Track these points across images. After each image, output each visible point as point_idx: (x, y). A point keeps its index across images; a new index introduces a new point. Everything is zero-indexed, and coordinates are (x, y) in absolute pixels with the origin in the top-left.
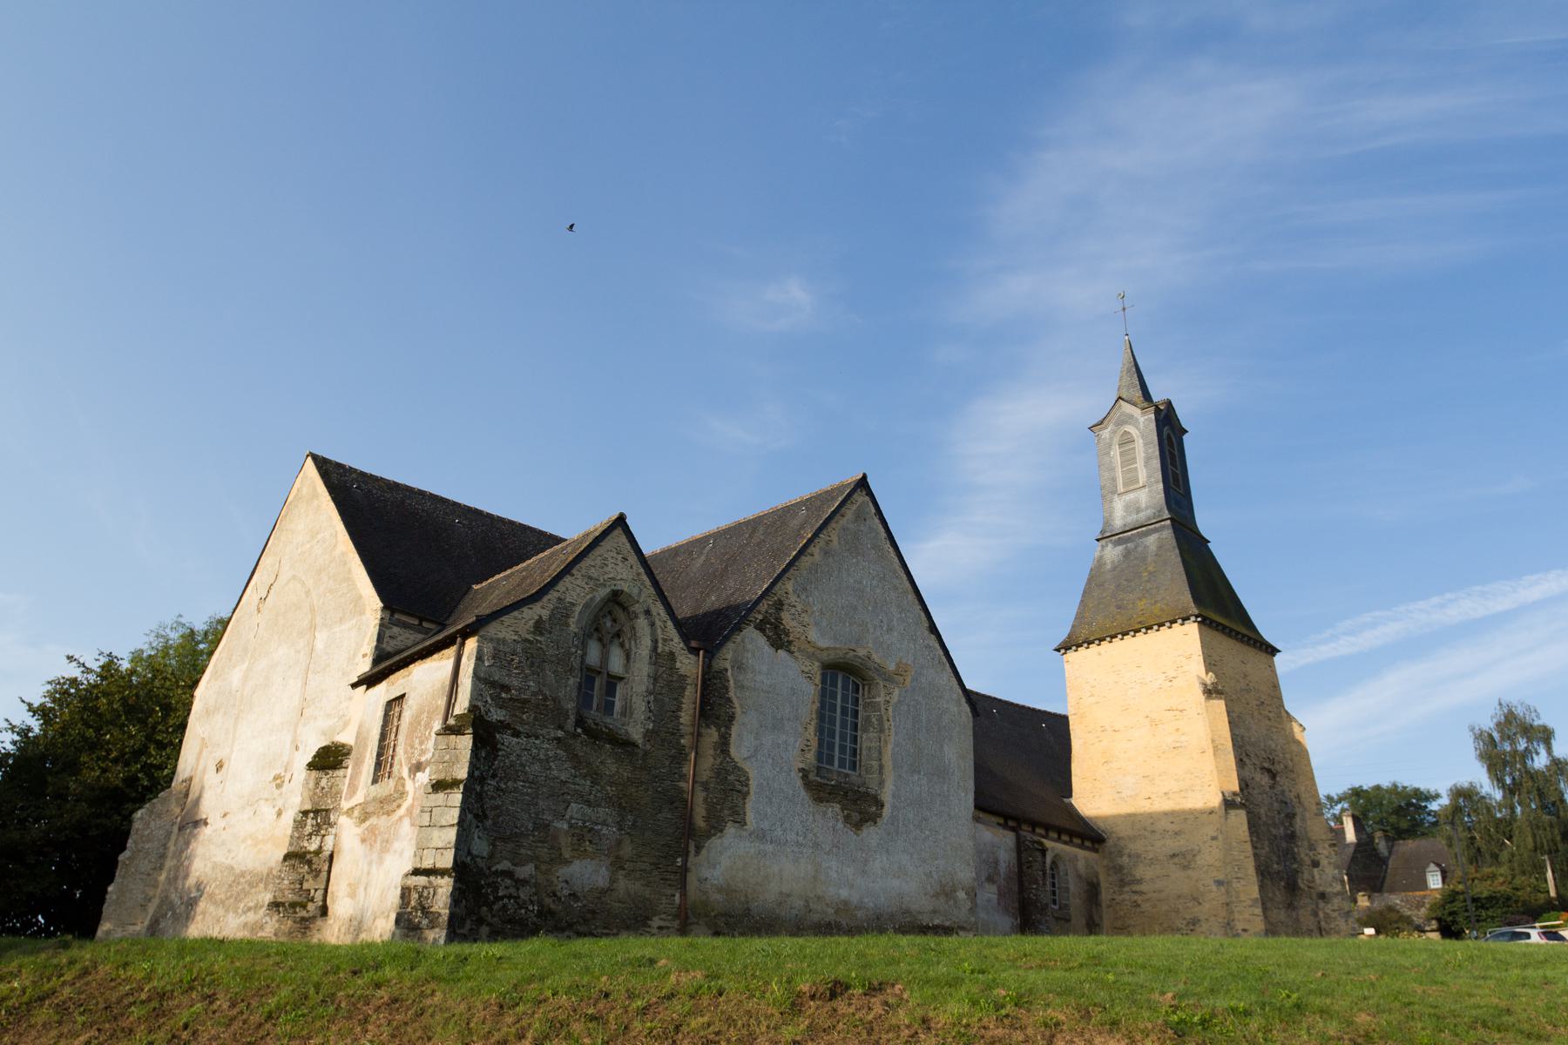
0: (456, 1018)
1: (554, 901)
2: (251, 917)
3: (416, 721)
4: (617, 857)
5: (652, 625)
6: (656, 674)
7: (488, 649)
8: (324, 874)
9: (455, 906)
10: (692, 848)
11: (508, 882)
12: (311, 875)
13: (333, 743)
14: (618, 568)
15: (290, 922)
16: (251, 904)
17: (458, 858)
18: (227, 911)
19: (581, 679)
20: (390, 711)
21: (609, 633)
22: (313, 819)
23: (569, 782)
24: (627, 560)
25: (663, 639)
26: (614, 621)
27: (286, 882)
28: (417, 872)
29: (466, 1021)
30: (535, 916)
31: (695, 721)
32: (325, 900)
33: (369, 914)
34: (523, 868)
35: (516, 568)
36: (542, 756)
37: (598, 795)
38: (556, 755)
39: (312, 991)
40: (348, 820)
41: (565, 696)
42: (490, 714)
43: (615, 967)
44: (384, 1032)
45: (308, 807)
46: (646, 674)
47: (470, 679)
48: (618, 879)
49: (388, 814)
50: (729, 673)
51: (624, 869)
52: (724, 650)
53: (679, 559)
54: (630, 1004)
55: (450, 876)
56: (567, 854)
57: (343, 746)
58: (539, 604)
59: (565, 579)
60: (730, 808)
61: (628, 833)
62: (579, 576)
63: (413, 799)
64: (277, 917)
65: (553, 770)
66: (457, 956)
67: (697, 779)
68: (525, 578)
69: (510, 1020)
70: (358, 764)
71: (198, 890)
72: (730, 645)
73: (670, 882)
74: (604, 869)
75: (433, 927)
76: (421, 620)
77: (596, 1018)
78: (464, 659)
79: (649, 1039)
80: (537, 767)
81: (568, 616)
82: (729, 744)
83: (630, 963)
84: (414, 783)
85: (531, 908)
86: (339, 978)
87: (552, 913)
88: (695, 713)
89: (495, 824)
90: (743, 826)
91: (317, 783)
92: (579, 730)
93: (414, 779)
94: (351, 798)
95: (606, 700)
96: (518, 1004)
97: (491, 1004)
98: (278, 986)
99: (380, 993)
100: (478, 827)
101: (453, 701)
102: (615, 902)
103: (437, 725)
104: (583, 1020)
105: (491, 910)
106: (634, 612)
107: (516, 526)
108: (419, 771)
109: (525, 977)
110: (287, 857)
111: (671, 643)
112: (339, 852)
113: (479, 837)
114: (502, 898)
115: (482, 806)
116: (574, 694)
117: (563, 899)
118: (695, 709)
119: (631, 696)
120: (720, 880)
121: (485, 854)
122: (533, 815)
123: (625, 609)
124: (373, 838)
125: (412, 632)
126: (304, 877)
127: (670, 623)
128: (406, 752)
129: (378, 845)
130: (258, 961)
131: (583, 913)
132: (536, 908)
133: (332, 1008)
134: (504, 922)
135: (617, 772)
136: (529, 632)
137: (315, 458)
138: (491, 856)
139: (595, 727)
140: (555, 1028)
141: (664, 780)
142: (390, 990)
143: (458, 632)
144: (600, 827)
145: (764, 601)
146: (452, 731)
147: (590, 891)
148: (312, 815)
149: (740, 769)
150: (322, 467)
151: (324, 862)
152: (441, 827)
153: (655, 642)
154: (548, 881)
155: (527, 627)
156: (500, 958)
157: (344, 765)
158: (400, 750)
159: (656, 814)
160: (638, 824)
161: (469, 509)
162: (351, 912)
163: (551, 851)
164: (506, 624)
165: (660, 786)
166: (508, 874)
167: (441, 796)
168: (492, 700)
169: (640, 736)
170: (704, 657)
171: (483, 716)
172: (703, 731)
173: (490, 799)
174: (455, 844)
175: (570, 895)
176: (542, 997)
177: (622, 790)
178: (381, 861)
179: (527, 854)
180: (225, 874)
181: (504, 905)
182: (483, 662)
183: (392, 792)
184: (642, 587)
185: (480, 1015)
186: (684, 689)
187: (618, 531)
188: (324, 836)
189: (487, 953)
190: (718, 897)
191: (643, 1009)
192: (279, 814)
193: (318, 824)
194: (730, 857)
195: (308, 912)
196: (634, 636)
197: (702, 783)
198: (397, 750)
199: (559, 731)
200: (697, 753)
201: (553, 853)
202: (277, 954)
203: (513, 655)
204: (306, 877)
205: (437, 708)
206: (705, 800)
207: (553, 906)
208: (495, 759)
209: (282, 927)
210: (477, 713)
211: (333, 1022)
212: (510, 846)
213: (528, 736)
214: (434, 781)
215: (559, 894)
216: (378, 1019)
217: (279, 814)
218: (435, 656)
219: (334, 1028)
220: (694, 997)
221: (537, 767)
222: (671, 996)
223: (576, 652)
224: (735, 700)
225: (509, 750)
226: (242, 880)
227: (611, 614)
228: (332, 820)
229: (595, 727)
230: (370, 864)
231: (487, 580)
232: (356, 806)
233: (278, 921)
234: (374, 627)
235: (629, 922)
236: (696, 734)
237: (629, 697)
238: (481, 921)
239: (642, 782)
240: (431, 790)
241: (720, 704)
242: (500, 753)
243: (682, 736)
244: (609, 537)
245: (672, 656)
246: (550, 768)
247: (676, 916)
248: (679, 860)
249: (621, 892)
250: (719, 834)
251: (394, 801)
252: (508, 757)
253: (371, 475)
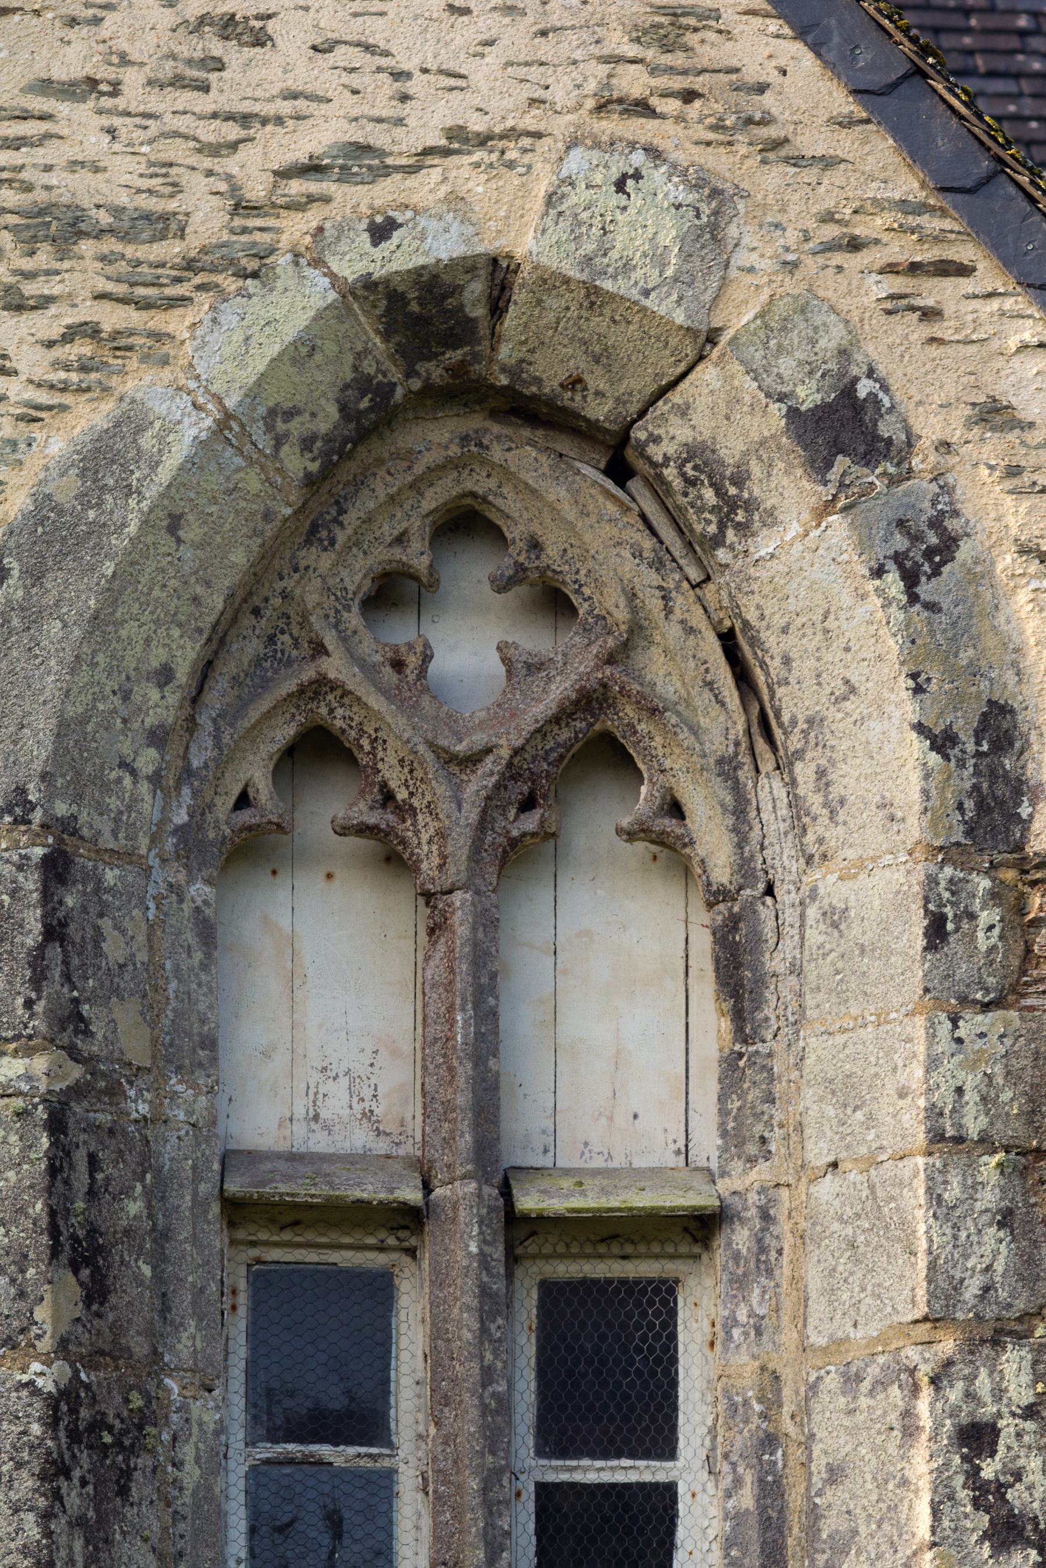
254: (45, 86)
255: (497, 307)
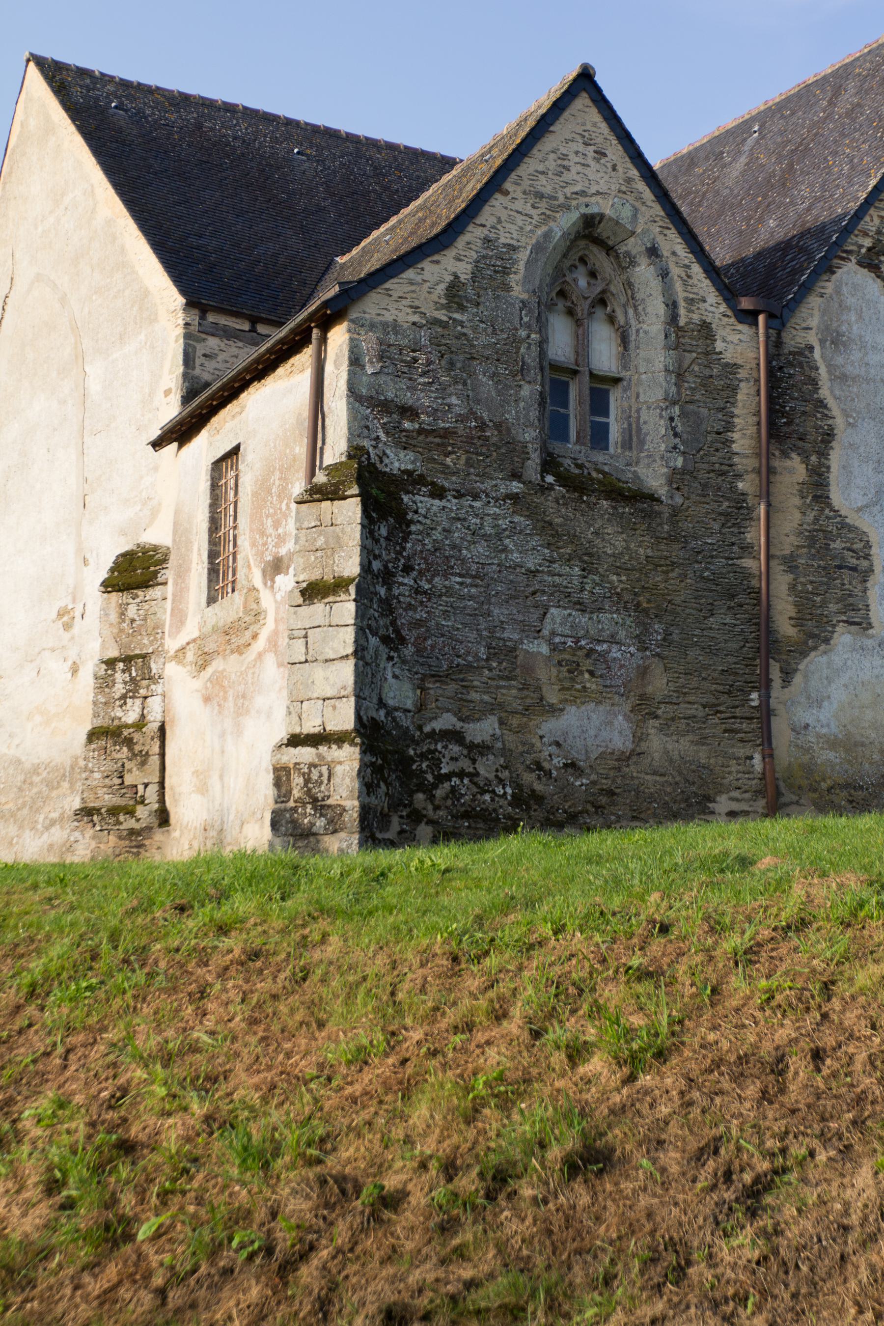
0: (368, 984)
1: (539, 778)
2: (58, 835)
3: (263, 488)
4: (642, 697)
5: (664, 274)
6: (680, 366)
7: (369, 343)
8: (155, 760)
9: (368, 794)
10: (775, 674)
11: (455, 749)
12: (134, 762)
13: (138, 545)
14: (587, 171)
15: (112, 838)
16: (55, 815)
17: (362, 713)
18: (21, 827)
19: (542, 385)
20: (220, 479)
21: (586, 298)
22: (124, 671)
23: (542, 572)
24: (605, 155)
25: (686, 299)
26: (593, 274)
27: (97, 775)
28: (295, 741)
29: (389, 989)
30: (510, 804)
31: (760, 447)
32: (162, 800)
33: (232, 817)
34: (478, 725)
35: (405, 212)
36: (488, 530)
37: (597, 590)
38: (513, 525)
39: (105, 947)
40: (179, 668)
41: (518, 419)
42: (386, 461)
43: (673, 875)
44: (235, 1013)
45: (114, 653)
46: (661, 366)
47: (344, 400)
48: (648, 735)
49: (240, 650)
50: (817, 354)
51: (657, 717)
52: (803, 311)
53: (698, 171)
54: (716, 943)
55: (352, 744)
56: (552, 697)
57: (155, 548)
58: (451, 253)
59: (493, 202)
60: (839, 601)
61: (658, 655)
62: (519, 195)
63: (276, 620)
64: (92, 831)
65: (512, 552)
66: (366, 871)
67: (773, 551)
68: (421, 220)
69: (473, 984)
70: (182, 573)
71: (750, 977)
72: (814, 301)
73: (743, 735)
74: (620, 718)
75: (335, 831)
76: (254, 321)
77: (649, 975)
78: (329, 368)
79: (768, 1012)
80: (481, 548)
81: (506, 272)
82: (828, 485)
83: (702, 866)
84: (274, 595)
85: (500, 791)
86: (154, 919)
87: (539, 798)
88: (759, 431)
89: (419, 651)
90: (867, 629)
91: (123, 614)
92: (550, 479)
93: (272, 587)
94: (178, 632)
95: (592, 422)
96: (487, 953)
97: (435, 955)
98: (48, 937)
99: (227, 942)
100: (390, 658)
101: (319, 444)
102: (647, 774)
103: (298, 487)
104: (623, 979)
105: (431, 798)
106: (628, 254)
107: (400, 152)
108: (279, 573)
109: (496, 901)
110: (93, 735)
111: (701, 305)
112: (173, 722)
113: (395, 677)
114: (448, 777)
115: (393, 623)
116: (534, 414)
117: (555, 773)
118: (759, 424)
119: (638, 411)
120: (833, 726)
121: (409, 704)
122: (485, 633)
123: (609, 250)
124: (222, 694)
125: (240, 344)
126: (123, 765)
127: (697, 269)
128: (253, 544)
129: (230, 703)
130: (15, 897)
131: (593, 795)
132: (509, 790)
133: (140, 977)
134: (457, 818)
135: (627, 548)
136: (439, 307)
137: (41, 63)
138: (421, 707)
139: (577, 471)
140: (567, 996)
141: (712, 557)
142: (244, 936)
143: (311, 318)
144: (605, 646)
145: (872, 211)
146: (323, 495)
147: (601, 756)
148: (121, 665)
149: (851, 528)
150: (54, 77)
151: (152, 739)
152: (326, 661)
153: (672, 306)
154: (524, 744)
155: (434, 297)
156: (447, 871)
157: (159, 580)
158: (244, 542)
159: (705, 618)
160: (675, 637)
161: (315, 130)
162: (205, 816)
163: (526, 692)
164: (395, 295)
165: (707, 569)
166: (455, 736)
167: (318, 609)
168: (387, 433)
169: (662, 481)
170: (767, 327)
171: (374, 465)
172: (776, 463)
173: (405, 610)
174: (355, 689)
175: (566, 765)
176: (533, 938)
177: (639, 580)
178: (238, 730)
179: (482, 701)
180: (11, 772)
181: (453, 790)
182: (363, 367)
183: (241, 614)
184: (638, 204)
185: (413, 977)
186: (735, 390)
187: (583, 101)
188: (146, 698)
189: (422, 862)
190: (831, 755)
191: (745, 953)
192: (75, 670)
193: (133, 680)
194: (845, 686)
195: (138, 820)
196: (632, 301)
197: (784, 557)
198: (239, 542)
199: (514, 483)
200: (769, 505)
201: (526, 697)
202: (48, 882)
203: (414, 351)
204: (127, 766)
205: (294, 460)
206: (792, 587)
207: (538, 787)
208: (405, 539)
209: (102, 846)
210: (363, 459)
211: (144, 999)
212: (452, 688)
213: (459, 495)
214: (304, 585)
215: (546, 765)
216: (225, 990)
217: (75, 670)
218: (280, 371)
219: (146, 1010)
220: (849, 925)
221: (481, 548)
222: (802, 925)
223: (529, 337)
224: (830, 402)
225: (428, 522)
226: (36, 779)
227: (586, 263)
228: (154, 671)
229: (577, 471)
230: (223, 735)
231: (359, 244)
232: (188, 644)
233: (93, 837)
234: (176, 341)
235: (675, 807)
236: (764, 469)
237: (633, 414)
238: (416, 817)
239: (673, 563)
240: (300, 600)
241: (804, 413)
242: (413, 528)
243: (739, 476)
244: (566, 114)
245: (706, 330)
246: (505, 550)
247: (759, 793)
248: (754, 695)
249: (657, 756)
250: (823, 647)
251: (247, 629)
252: (428, 534)
253: (139, 84)
254: (537, 171)
255: (600, 222)
